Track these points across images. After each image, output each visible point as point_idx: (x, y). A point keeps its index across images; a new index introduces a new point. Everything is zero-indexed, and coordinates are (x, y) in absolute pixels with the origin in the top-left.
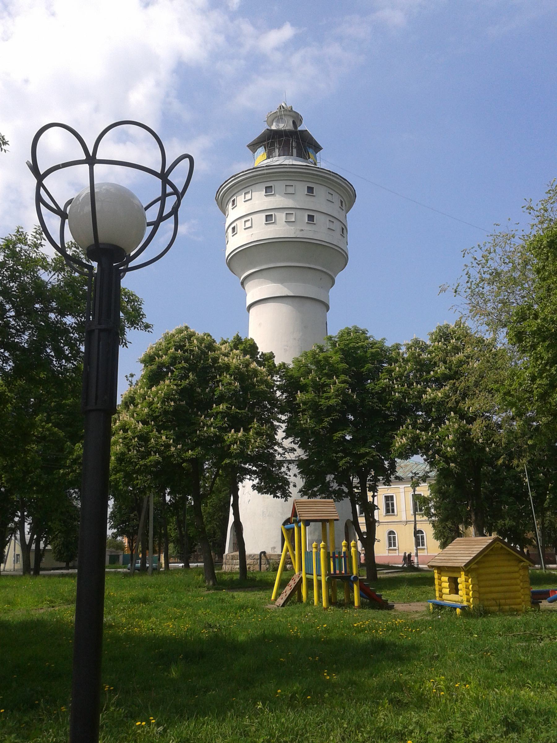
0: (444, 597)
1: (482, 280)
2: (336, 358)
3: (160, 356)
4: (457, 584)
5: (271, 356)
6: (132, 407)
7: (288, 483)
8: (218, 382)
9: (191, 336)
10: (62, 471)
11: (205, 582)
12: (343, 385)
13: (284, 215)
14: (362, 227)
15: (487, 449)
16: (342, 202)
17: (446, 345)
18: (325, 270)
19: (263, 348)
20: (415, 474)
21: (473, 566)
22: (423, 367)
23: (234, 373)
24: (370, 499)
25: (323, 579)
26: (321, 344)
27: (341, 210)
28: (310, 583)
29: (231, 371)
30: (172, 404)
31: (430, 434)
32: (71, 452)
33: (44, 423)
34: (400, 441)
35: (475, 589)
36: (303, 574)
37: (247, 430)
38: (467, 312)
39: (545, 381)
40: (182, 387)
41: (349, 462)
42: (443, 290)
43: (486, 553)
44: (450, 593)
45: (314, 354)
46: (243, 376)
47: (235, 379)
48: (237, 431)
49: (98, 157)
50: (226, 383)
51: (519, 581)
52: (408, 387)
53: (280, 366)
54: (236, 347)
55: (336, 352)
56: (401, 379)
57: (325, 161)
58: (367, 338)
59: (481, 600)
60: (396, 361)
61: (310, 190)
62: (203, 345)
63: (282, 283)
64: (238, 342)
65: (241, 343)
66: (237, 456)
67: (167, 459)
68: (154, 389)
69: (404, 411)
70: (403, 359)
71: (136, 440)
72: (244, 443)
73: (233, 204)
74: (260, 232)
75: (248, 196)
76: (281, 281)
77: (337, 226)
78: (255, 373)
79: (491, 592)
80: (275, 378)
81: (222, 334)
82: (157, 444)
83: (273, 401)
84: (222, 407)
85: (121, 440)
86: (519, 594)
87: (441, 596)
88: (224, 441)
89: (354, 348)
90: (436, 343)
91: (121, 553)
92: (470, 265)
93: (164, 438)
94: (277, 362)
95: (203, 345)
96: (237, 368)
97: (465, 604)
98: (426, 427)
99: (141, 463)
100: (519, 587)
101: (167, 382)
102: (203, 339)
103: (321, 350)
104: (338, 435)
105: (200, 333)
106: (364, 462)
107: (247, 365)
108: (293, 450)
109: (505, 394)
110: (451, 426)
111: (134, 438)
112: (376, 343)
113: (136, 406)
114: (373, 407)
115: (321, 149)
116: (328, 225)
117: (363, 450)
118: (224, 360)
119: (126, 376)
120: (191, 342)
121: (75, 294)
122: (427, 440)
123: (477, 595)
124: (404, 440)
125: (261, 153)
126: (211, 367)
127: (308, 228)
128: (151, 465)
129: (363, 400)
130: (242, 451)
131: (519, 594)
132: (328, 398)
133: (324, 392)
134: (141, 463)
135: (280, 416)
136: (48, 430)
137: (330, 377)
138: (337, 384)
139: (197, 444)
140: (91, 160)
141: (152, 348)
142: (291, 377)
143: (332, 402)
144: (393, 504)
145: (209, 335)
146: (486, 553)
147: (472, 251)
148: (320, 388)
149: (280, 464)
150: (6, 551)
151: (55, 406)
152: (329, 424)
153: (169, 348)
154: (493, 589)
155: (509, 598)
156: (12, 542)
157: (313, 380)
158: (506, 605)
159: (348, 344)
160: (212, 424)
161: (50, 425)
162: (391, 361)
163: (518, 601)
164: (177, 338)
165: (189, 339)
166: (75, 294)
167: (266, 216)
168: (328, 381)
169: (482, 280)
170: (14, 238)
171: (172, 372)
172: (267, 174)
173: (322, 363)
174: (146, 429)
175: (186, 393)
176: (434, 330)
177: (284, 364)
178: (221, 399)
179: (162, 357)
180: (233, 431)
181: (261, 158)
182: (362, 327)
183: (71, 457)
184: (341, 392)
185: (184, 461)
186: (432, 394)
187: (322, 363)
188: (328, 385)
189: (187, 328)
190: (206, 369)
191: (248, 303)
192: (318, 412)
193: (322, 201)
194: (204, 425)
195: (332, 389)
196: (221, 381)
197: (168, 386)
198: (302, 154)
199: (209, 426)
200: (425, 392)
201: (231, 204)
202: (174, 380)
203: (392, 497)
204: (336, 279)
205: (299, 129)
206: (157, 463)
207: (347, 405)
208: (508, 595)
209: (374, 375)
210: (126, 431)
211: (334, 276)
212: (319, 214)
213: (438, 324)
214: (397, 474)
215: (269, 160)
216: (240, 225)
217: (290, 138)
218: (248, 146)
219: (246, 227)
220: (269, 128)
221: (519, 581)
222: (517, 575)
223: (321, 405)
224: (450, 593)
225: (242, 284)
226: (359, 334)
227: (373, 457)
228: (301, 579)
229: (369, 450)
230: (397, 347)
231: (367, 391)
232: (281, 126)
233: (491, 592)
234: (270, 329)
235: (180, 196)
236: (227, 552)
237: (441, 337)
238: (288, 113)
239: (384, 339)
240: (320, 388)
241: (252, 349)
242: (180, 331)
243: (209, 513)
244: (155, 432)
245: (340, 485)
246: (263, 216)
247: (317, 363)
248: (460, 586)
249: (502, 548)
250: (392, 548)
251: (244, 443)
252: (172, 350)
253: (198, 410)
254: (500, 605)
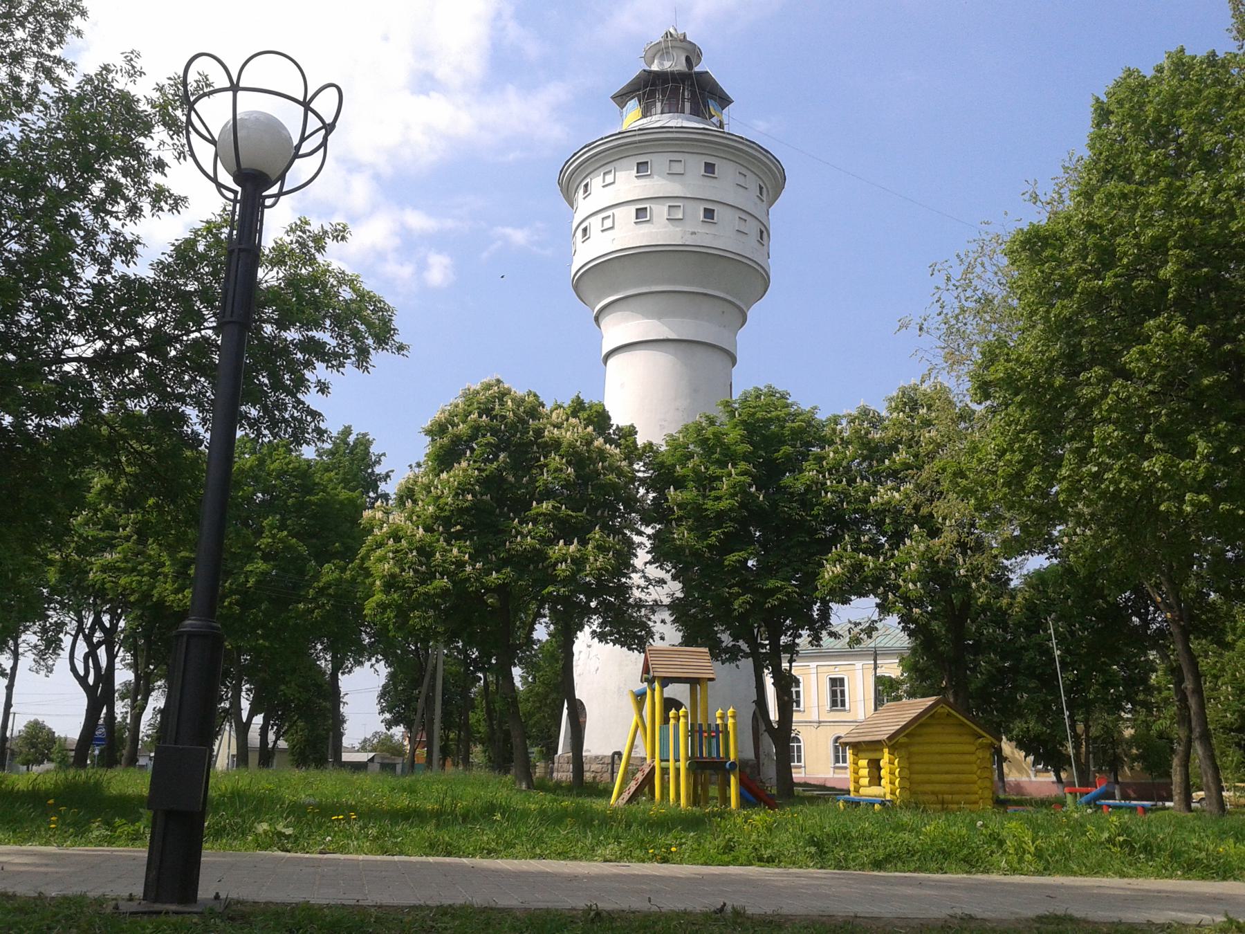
0: (862, 791)
1: (963, 310)
2: (734, 435)
3: (454, 425)
4: (880, 769)
5: (632, 431)
6: (409, 504)
7: (650, 634)
8: (541, 467)
9: (503, 394)
10: (301, 606)
11: (514, 783)
12: (742, 478)
13: (666, 209)
14: (796, 234)
15: (974, 585)
16: (761, 188)
17: (912, 417)
18: (729, 298)
19: (619, 419)
20: (856, 624)
21: (902, 739)
22: (874, 452)
23: (567, 454)
24: (785, 665)
25: (683, 765)
26: (712, 414)
27: (758, 201)
28: (665, 771)
29: (562, 451)
30: (470, 497)
31: (881, 559)
32: (317, 577)
33: (275, 531)
34: (831, 571)
35: (904, 774)
36: (657, 763)
37: (583, 542)
38: (939, 361)
39: (1018, 456)
40: (487, 473)
41: (748, 602)
42: (904, 326)
43: (920, 721)
44: (871, 784)
45: (699, 429)
46: (581, 459)
47: (569, 463)
48: (568, 543)
49: (241, 85)
50: (554, 470)
51: (975, 768)
52: (849, 484)
53: (645, 447)
54: (574, 414)
55: (736, 426)
56: (837, 471)
57: (738, 121)
58: (787, 406)
59: (913, 793)
60: (832, 443)
61: (710, 168)
62: (522, 409)
63: (659, 319)
64: (578, 407)
65: (584, 409)
66: (566, 581)
67: (460, 583)
68: (444, 476)
69: (842, 522)
70: (842, 439)
71: (415, 553)
72: (579, 562)
73: (585, 191)
74: (626, 235)
75: (609, 178)
76: (659, 315)
77: (752, 227)
78: (602, 455)
79: (932, 782)
80: (636, 467)
81: (555, 394)
82: (444, 561)
83: (631, 503)
84: (546, 506)
85: (391, 555)
86: (975, 788)
87: (857, 791)
88: (546, 557)
89: (764, 420)
90: (895, 414)
91: (399, 760)
92: (943, 286)
93: (455, 551)
94: (641, 440)
95: (522, 409)
96: (571, 445)
97: (888, 797)
98: (875, 550)
99: (421, 589)
100: (975, 777)
101: (464, 464)
102: (523, 400)
103: (712, 422)
104: (732, 558)
105: (519, 391)
106: (772, 602)
107: (589, 443)
108: (662, 582)
109: (955, 474)
110: (915, 545)
111: (411, 551)
112: (800, 414)
113: (415, 502)
114: (790, 515)
115: (731, 102)
116: (738, 225)
117: (772, 583)
118: (550, 433)
119: (410, 466)
120: (502, 404)
121: (300, 298)
122: (875, 568)
123: (907, 785)
124: (838, 569)
125: (633, 110)
126: (531, 443)
128: (436, 595)
129: (774, 505)
130: (574, 574)
131: (975, 788)
132: (718, 498)
133: (713, 489)
134: (421, 589)
135: (643, 529)
136: (281, 541)
137: (723, 465)
138: (733, 476)
139: (505, 563)
140: (235, 88)
141: (443, 412)
142: (662, 465)
143: (724, 504)
144: (843, 693)
145: (535, 395)
146: (920, 721)
147: (946, 265)
148: (706, 483)
149: (639, 604)
150: (216, 748)
151: (293, 505)
152: (719, 540)
153: (470, 413)
154: (933, 777)
155: (958, 793)
156: (226, 734)
157: (695, 470)
158: (952, 803)
159: (754, 414)
160: (529, 532)
161: (285, 533)
162: (824, 442)
163: (973, 797)
164: (482, 398)
165: (501, 400)
166: (300, 298)
167: (637, 210)
168: (719, 472)
169: (963, 310)
170: (219, 219)
171: (472, 450)
172: (640, 142)
173: (711, 443)
174: (429, 538)
175: (491, 483)
176: (895, 394)
177: (651, 444)
178: (548, 494)
179: (458, 425)
180: (561, 542)
181: (632, 117)
182: (780, 388)
183: (315, 584)
184: (739, 490)
185: (489, 590)
186: (885, 494)
187: (711, 443)
188: (719, 478)
189: (499, 381)
190: (524, 447)
191: (605, 351)
192: (701, 520)
193: (727, 185)
194: (518, 533)
195: (725, 485)
196: (546, 465)
197: (465, 470)
198: (699, 111)
199: (526, 536)
200: (874, 493)
201: (581, 191)
202: (475, 462)
203: (842, 680)
204: (749, 314)
205: (697, 69)
206: (445, 593)
207: (749, 513)
208: (957, 788)
209: (794, 464)
210: (398, 539)
213: (902, 383)
214: (833, 629)
215: (645, 120)
216: (595, 224)
217: (678, 85)
218: (613, 98)
220: (647, 68)
221: (975, 768)
222: (973, 758)
223: (707, 510)
224: (871, 784)
225: (597, 319)
226: (776, 399)
227: (788, 594)
228: (653, 768)
229: (784, 586)
230: (836, 420)
231: (782, 490)
232: (667, 66)
233: (932, 782)
234: (641, 397)
235: (329, 128)
236: (560, 752)
237: (905, 404)
238: (678, 44)
239: (816, 408)
240: (706, 483)
241: (600, 419)
242: (488, 387)
243: (537, 694)
244: (442, 543)
245: (736, 639)
246: (632, 210)
247: (703, 442)
248: (883, 772)
249: (949, 715)
250: (841, 764)
251: (579, 562)
252: (474, 416)
253: (510, 511)
254: (943, 803)
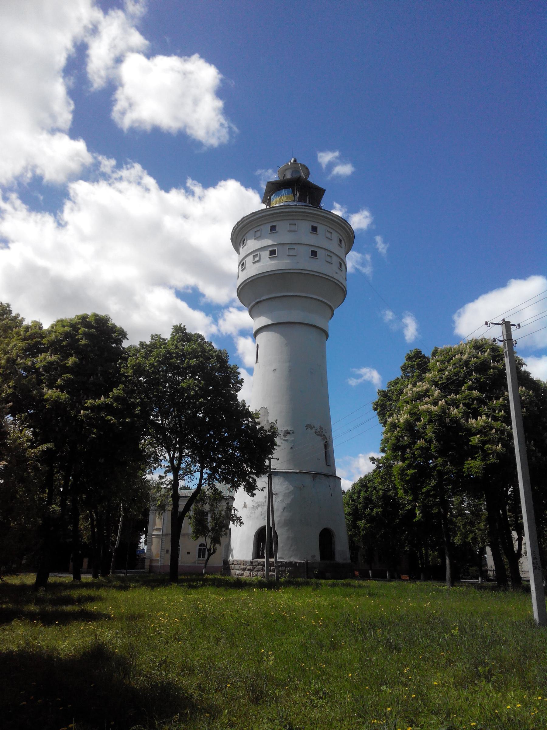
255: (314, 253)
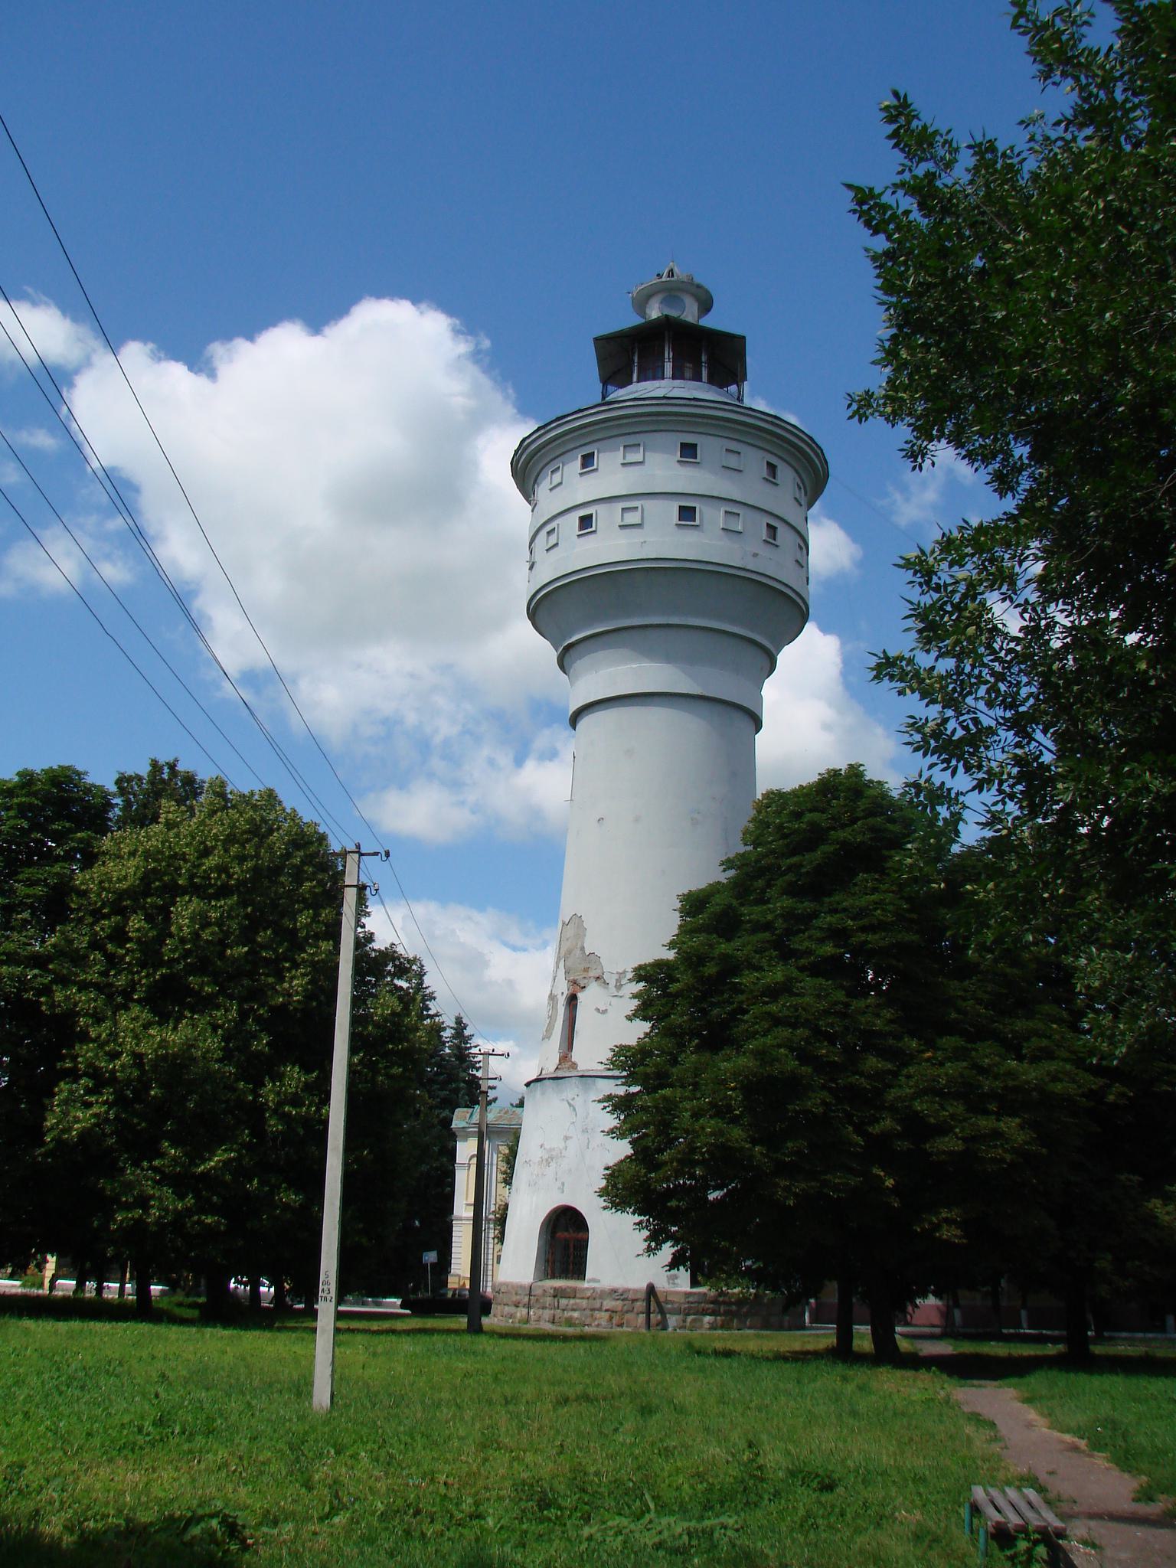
127: (765, 552)
211: (773, 650)
212: (787, 528)
219: (627, 521)
255: (687, 514)
